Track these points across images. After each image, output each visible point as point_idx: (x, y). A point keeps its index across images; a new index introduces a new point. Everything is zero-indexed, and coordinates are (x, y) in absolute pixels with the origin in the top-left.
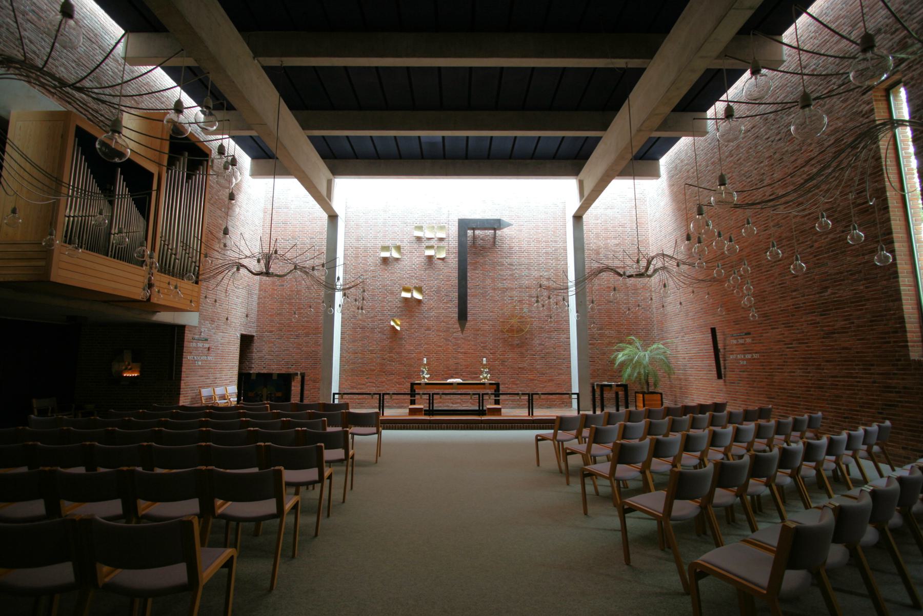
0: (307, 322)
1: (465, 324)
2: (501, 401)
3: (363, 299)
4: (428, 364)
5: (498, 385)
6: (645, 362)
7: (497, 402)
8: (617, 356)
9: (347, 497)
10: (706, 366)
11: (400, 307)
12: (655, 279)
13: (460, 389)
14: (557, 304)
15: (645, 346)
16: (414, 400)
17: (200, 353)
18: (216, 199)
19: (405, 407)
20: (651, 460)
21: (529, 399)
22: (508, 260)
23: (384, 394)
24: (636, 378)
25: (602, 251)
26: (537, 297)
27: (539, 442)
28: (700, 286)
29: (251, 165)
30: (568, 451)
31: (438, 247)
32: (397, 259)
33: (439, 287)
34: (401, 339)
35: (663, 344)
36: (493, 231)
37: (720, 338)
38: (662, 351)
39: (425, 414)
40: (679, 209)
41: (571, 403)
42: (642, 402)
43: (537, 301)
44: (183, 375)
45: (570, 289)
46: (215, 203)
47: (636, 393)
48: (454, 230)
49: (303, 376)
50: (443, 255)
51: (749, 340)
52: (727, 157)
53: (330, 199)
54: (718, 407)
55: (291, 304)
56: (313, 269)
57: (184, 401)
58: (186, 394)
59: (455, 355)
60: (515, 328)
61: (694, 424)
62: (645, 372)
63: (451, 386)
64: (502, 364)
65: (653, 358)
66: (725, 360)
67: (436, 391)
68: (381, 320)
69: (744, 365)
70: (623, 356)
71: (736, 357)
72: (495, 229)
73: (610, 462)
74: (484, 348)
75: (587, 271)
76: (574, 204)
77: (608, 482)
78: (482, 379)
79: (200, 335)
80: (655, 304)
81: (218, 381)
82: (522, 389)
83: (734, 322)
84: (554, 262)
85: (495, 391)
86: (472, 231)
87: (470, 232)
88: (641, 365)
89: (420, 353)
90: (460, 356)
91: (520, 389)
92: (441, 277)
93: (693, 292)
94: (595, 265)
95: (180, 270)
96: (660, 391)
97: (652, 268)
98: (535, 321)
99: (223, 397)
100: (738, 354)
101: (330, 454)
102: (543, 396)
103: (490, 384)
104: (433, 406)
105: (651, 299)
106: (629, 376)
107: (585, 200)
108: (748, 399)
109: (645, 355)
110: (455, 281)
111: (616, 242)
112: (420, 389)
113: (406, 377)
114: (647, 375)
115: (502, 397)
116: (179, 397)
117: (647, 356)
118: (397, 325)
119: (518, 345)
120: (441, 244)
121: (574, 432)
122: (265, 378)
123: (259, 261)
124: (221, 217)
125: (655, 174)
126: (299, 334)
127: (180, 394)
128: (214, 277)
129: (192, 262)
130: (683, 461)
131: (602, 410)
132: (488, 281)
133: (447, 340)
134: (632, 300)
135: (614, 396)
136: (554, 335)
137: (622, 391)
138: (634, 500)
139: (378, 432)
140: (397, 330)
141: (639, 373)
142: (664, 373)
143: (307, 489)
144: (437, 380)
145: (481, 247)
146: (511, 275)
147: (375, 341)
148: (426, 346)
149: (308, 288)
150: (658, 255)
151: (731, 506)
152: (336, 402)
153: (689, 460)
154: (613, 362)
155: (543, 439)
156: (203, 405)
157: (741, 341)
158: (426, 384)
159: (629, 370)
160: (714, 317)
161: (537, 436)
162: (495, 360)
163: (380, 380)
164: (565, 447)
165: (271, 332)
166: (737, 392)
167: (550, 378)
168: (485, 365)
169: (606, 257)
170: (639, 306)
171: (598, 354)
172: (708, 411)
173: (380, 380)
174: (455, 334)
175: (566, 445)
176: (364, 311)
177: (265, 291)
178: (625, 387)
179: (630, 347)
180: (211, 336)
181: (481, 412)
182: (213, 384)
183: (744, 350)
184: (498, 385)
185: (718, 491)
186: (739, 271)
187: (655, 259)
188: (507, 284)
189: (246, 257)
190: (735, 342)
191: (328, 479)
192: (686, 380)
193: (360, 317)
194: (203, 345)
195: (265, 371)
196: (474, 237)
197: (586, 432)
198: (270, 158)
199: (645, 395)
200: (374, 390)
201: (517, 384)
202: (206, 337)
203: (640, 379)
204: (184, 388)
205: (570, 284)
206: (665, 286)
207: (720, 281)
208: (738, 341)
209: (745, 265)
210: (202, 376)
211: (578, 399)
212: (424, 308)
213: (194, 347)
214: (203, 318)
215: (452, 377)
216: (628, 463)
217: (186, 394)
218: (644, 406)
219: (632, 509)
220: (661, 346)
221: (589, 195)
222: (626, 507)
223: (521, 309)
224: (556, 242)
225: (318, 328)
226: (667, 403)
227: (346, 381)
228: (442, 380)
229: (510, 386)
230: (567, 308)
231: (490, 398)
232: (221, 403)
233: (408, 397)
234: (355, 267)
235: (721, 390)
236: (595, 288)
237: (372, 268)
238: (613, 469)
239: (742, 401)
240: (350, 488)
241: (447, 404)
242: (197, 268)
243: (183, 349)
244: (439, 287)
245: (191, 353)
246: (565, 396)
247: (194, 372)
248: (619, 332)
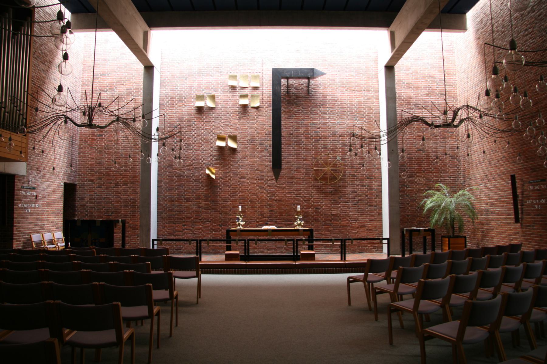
0: (125, 171)
1: (280, 172)
2: (314, 247)
3: (181, 149)
4: (243, 211)
5: (311, 231)
6: (451, 208)
7: (311, 248)
8: (425, 202)
9: (173, 332)
10: (506, 211)
11: (214, 156)
12: (462, 128)
13: (275, 235)
14: (369, 153)
15: (452, 192)
16: (230, 246)
17: (28, 201)
18: (39, 53)
19: (221, 253)
20: (450, 295)
21: (341, 244)
22: (322, 109)
23: (201, 241)
24: (443, 223)
25: (413, 101)
26: (350, 146)
27: (351, 284)
28: (503, 135)
29: (144, 78)
30: (377, 291)
31: (252, 96)
32: (212, 109)
34: (217, 187)
35: (468, 191)
36: (306, 80)
37: (518, 184)
38: (468, 197)
39: (241, 260)
40: (485, 62)
41: (382, 247)
42: (447, 245)
43: (350, 150)
44: (15, 221)
45: (382, 139)
46: (39, 57)
47: (443, 237)
48: (268, 80)
49: (124, 222)
50: (257, 104)
51: (543, 186)
52: (529, 13)
53: (146, 51)
54: (514, 248)
55: (109, 153)
56: (134, 121)
57: (17, 245)
58: (19, 239)
59: (269, 203)
61: (492, 263)
62: (451, 217)
64: (316, 212)
65: (459, 204)
66: (522, 205)
67: (251, 237)
68: (196, 168)
69: (538, 210)
70: (431, 202)
71: (532, 202)
72: (308, 78)
73: (414, 299)
74: (298, 195)
75: (399, 120)
76: (387, 54)
77: (411, 317)
78: (296, 226)
79: (28, 184)
80: (462, 152)
81: (46, 227)
82: (335, 235)
83: (531, 169)
84: (367, 111)
85: (309, 237)
86: (286, 80)
87: (284, 81)
88: (447, 211)
89: (236, 200)
90: (275, 203)
91: (333, 235)
92: (255, 126)
93: (495, 141)
94: (406, 115)
95: (15, 124)
96: (464, 235)
97: (458, 119)
98: (348, 169)
99: (51, 242)
100: (535, 199)
101: (159, 294)
102: (355, 242)
103: (304, 230)
104: (248, 252)
105: (458, 148)
106: (437, 221)
107: (396, 51)
108: (541, 240)
109: (451, 201)
110: (269, 129)
111: (426, 92)
112: (236, 235)
113: (222, 224)
114: (453, 220)
115: (315, 243)
116: (13, 242)
117: (453, 202)
118: (213, 173)
119: (331, 192)
120: (256, 93)
121: (384, 274)
122: (90, 224)
123: (84, 114)
124: (44, 71)
125: (461, 26)
126: (118, 183)
127: (13, 239)
128: (40, 129)
129: (20, 115)
130: (479, 296)
131: (411, 252)
132: (302, 130)
133: (262, 188)
134: (441, 149)
135: (422, 240)
136: (367, 182)
137: (429, 236)
138: (435, 329)
139: (198, 276)
140: (212, 178)
141: (446, 219)
142: (468, 217)
143: (137, 324)
145: (295, 96)
146: (325, 124)
147: (191, 189)
148: (241, 194)
149: (126, 138)
150: (463, 107)
151: (517, 330)
152: (156, 247)
153: (484, 294)
154: (422, 208)
155: (355, 280)
156: (34, 249)
157: (537, 187)
158: (242, 231)
159: (436, 216)
160: (514, 165)
161: (349, 278)
162: (309, 207)
163: (196, 227)
164: (374, 287)
165: (92, 180)
166: (532, 234)
167: (362, 224)
168: (299, 212)
169: (417, 106)
170: (446, 154)
171: (408, 200)
172: (504, 252)
173: (196, 227)
174: (269, 182)
175: (376, 285)
176: (181, 161)
177: (85, 141)
178: (432, 232)
179: (439, 193)
180: (38, 185)
181: (296, 257)
182: (41, 231)
183: (539, 196)
184: (311, 231)
185: (505, 318)
186: (535, 122)
187: (461, 110)
188: (320, 132)
189: (72, 110)
190: (531, 188)
191: (156, 315)
192: (488, 224)
193: (178, 165)
194: (31, 194)
195: (87, 218)
196: (288, 86)
197: (394, 274)
198: (89, 12)
199: (451, 239)
200: (190, 236)
201: (330, 231)
202: (34, 186)
203: (447, 224)
204: (16, 234)
205: (382, 133)
206: (468, 136)
207: (520, 132)
208: (534, 188)
209: (540, 117)
210: (32, 223)
211: (388, 244)
212: (239, 156)
213: (24, 196)
214: (30, 168)
215: (267, 224)
216: (429, 299)
217: (19, 239)
218: (449, 249)
219: (431, 336)
220: (467, 193)
221: (400, 46)
222: (426, 335)
223: (335, 157)
224: (368, 91)
225: (135, 177)
226: (470, 245)
227: (164, 228)
228: (257, 226)
230: (378, 157)
231: (304, 244)
232: (50, 247)
233: (225, 244)
234: (171, 117)
235: (518, 233)
236: (407, 136)
237: (187, 118)
238: (416, 305)
239: (536, 242)
240: (175, 325)
241: (262, 250)
242: (24, 120)
243: (14, 197)
245: (21, 200)
246: (376, 241)
247: (24, 218)
248: (428, 179)
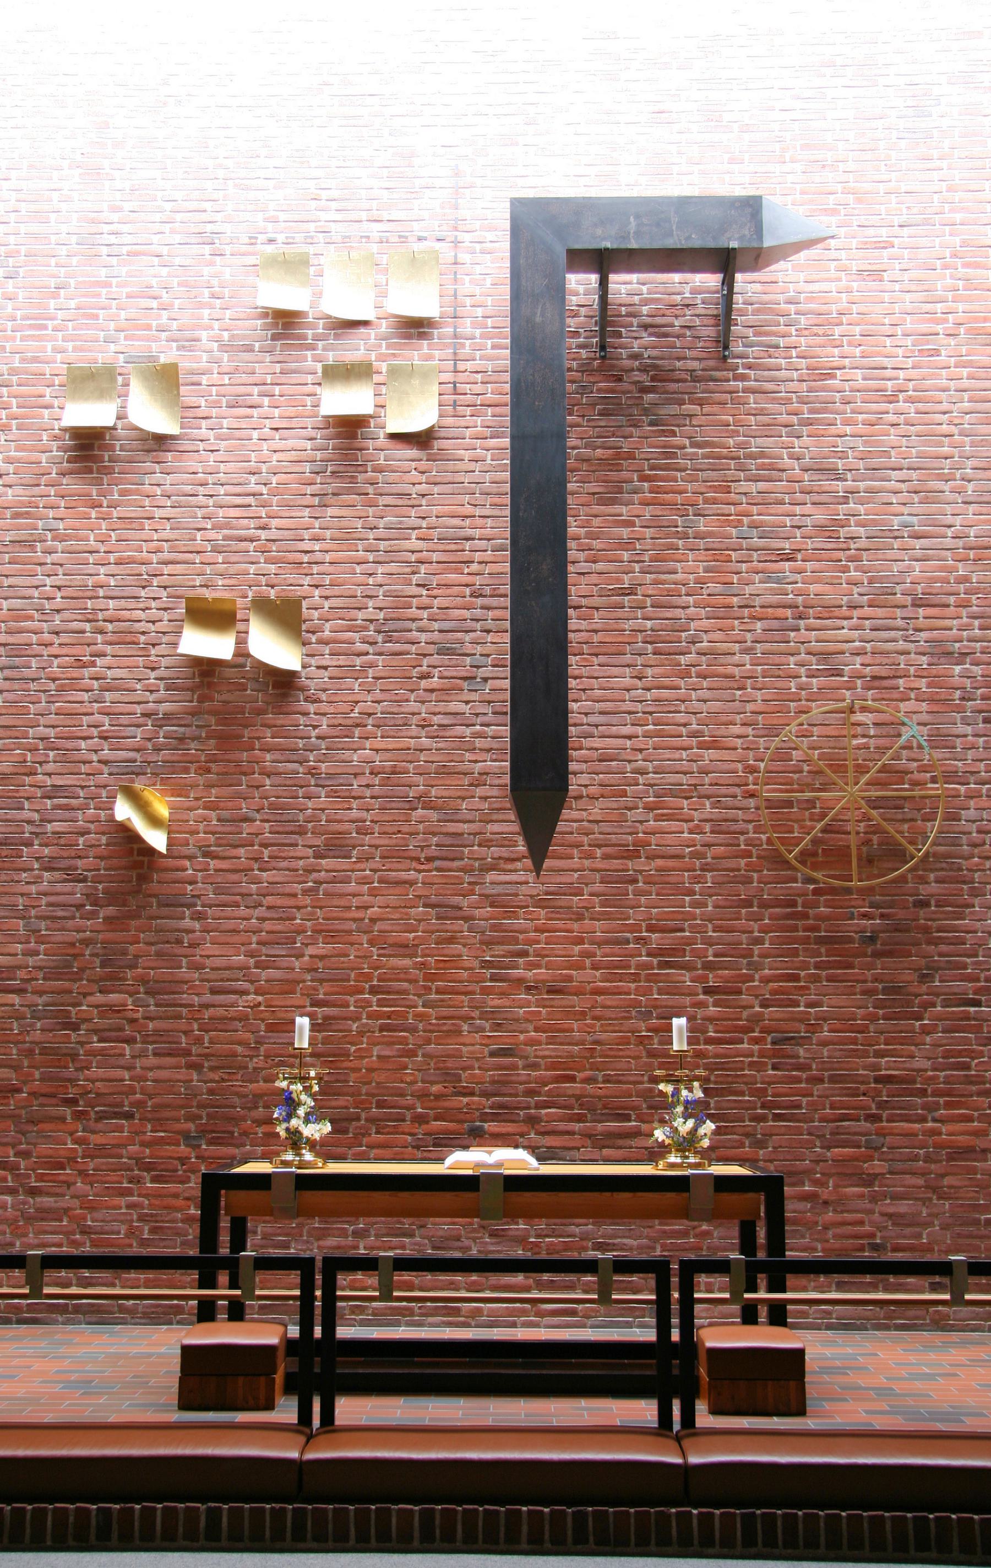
11: (168, 717)
22: (805, 444)
31: (393, 371)
32: (160, 442)
33: (402, 601)
34: (174, 903)
36: (711, 280)
59: (493, 1001)
60: (853, 841)
63: (467, 1197)
68: (57, 790)
86: (594, 278)
89: (288, 986)
91: (889, 1206)
92: (414, 544)
103: (723, 1183)
118: (154, 821)
140: (151, 851)
144: (93, 1305)
145: (644, 369)
146: (828, 530)
148: (321, 948)
174: (491, 877)
201: (869, 1180)
215: (476, 1137)
223: (891, 728)
229: (825, 1193)
244: (402, 601)
